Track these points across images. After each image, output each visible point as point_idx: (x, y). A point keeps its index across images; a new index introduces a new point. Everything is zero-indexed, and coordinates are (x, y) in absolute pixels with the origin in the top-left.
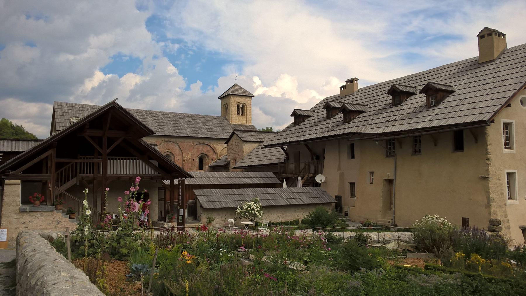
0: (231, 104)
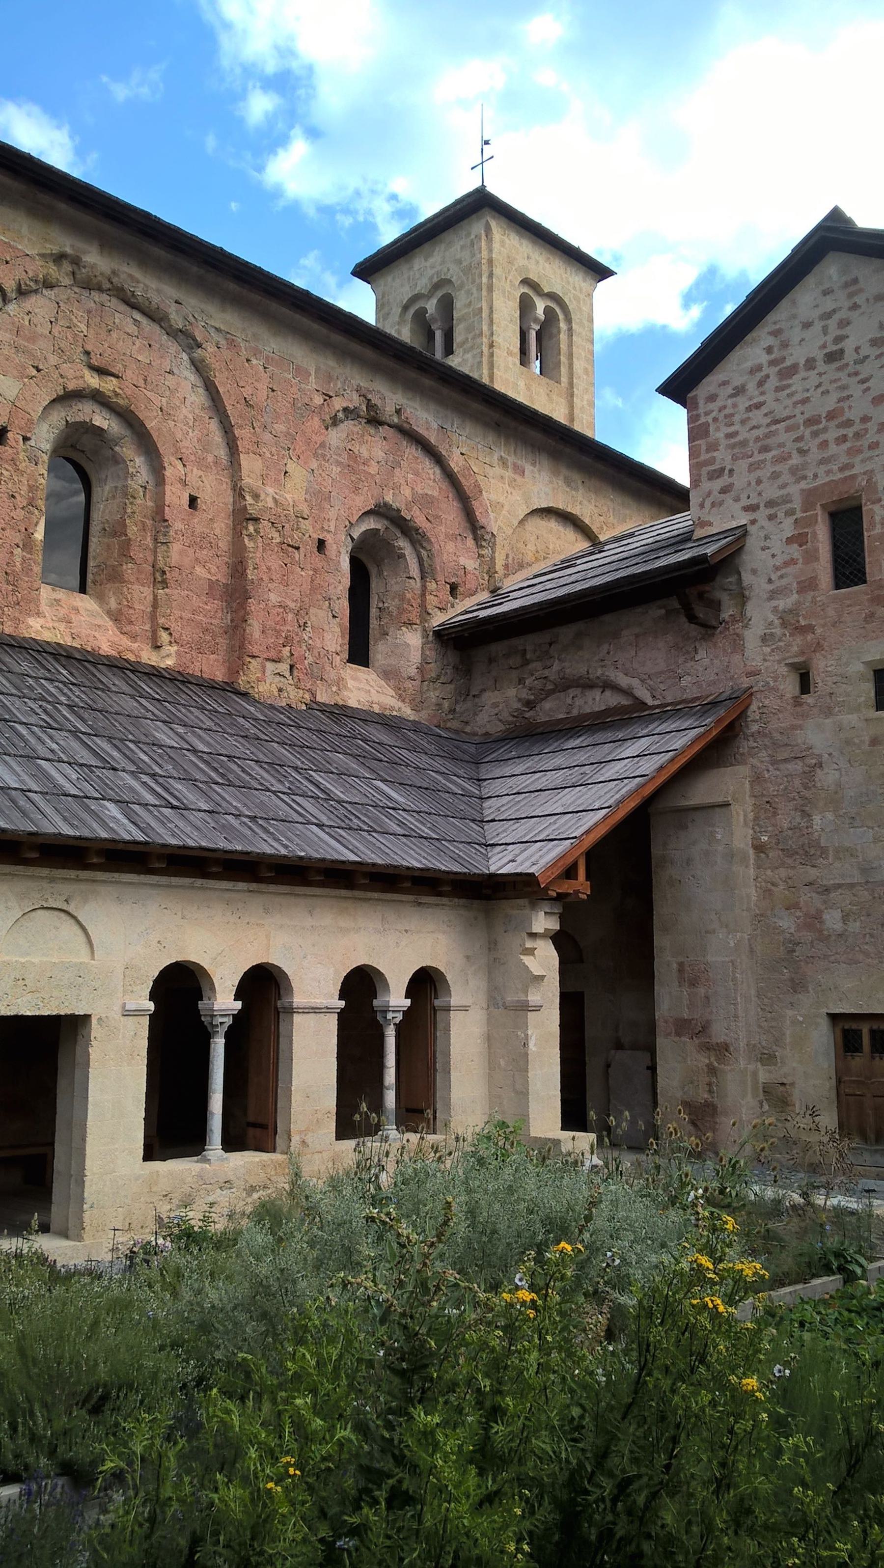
0: (491, 276)
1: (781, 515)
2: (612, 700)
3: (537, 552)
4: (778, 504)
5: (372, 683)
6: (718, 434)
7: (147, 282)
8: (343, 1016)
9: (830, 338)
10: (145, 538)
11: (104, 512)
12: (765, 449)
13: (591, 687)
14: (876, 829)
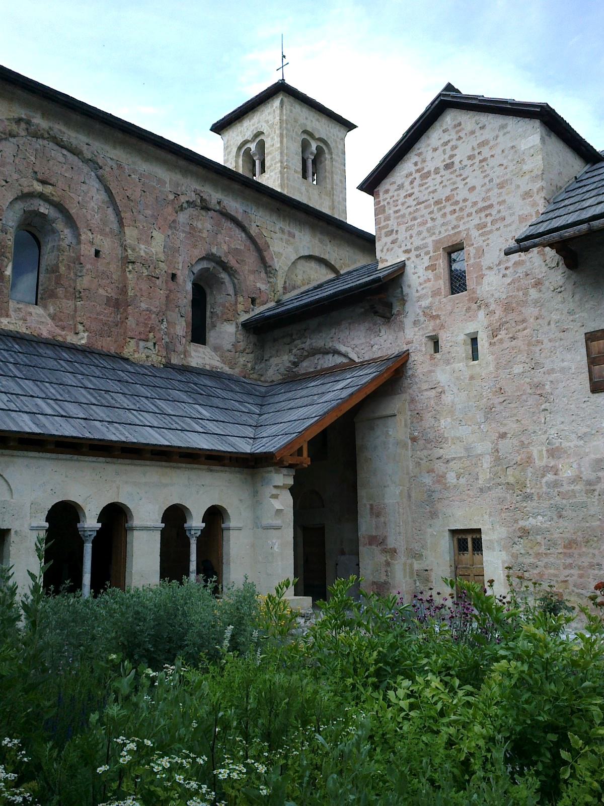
1: (422, 254)
2: (339, 360)
3: (304, 280)
4: (421, 249)
5: (207, 354)
6: (390, 211)
7: (69, 133)
8: (163, 532)
9: (447, 156)
10: (70, 274)
11: (47, 259)
12: (415, 219)
13: (327, 353)
14: (473, 426)
